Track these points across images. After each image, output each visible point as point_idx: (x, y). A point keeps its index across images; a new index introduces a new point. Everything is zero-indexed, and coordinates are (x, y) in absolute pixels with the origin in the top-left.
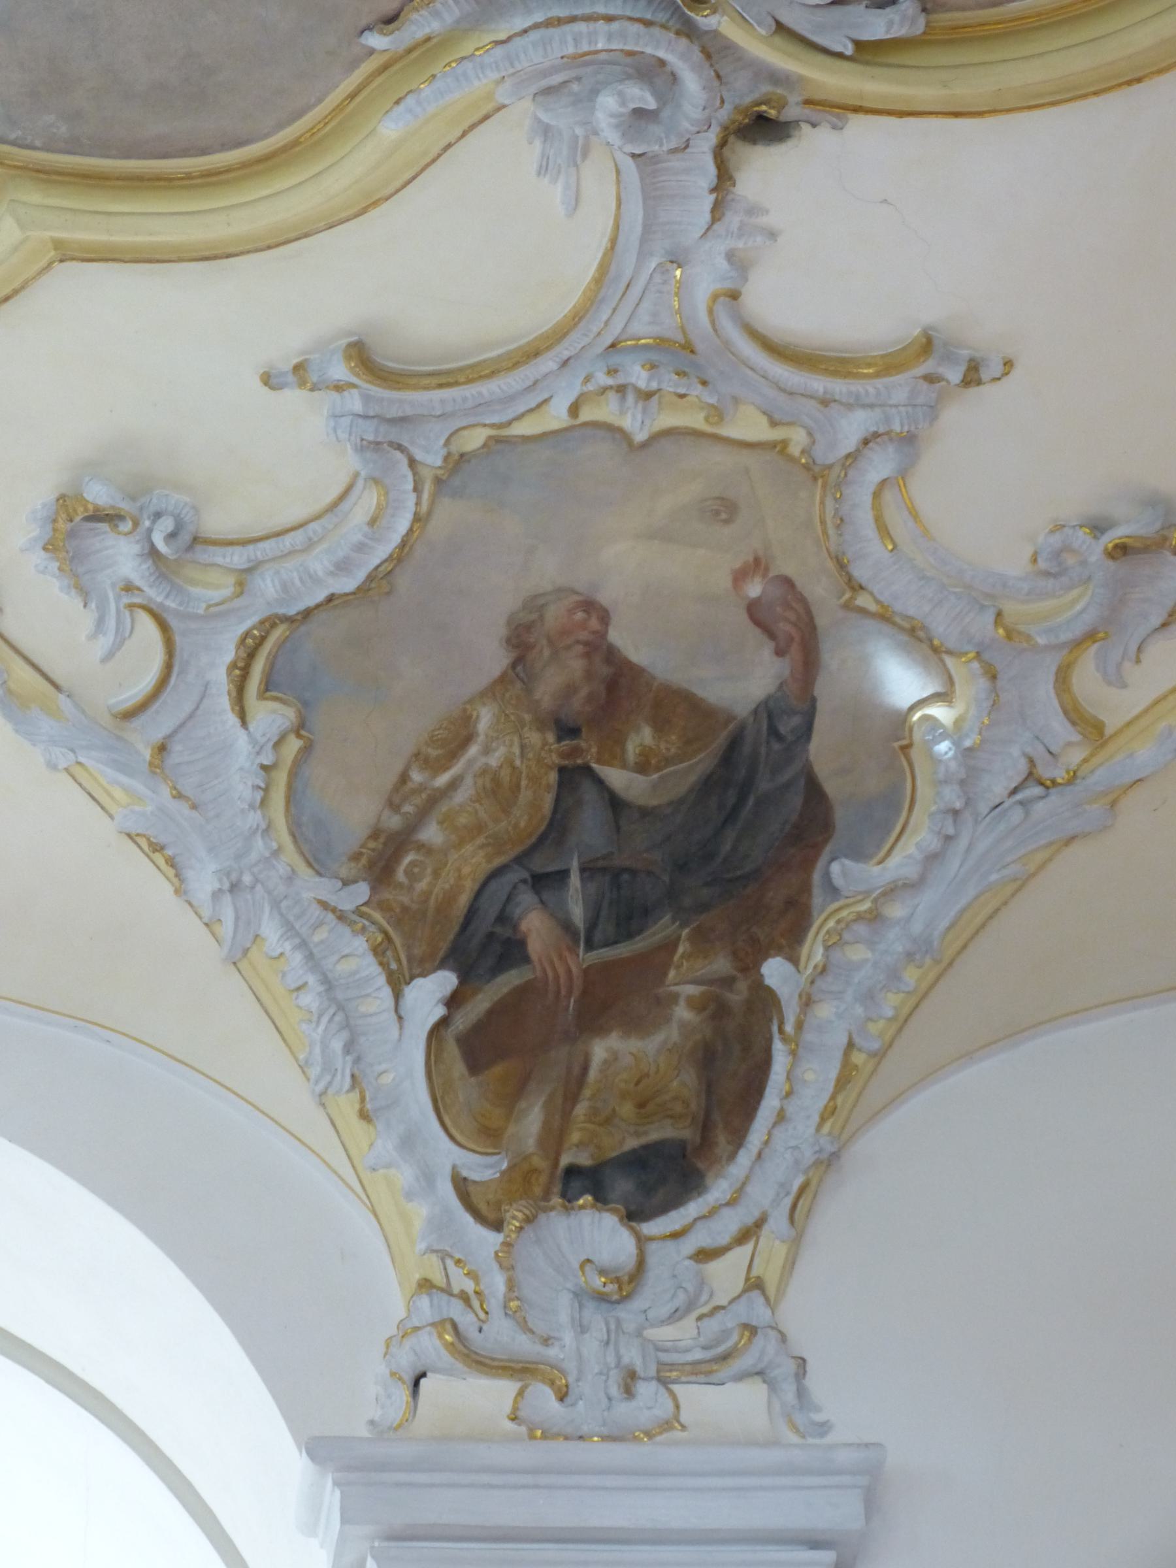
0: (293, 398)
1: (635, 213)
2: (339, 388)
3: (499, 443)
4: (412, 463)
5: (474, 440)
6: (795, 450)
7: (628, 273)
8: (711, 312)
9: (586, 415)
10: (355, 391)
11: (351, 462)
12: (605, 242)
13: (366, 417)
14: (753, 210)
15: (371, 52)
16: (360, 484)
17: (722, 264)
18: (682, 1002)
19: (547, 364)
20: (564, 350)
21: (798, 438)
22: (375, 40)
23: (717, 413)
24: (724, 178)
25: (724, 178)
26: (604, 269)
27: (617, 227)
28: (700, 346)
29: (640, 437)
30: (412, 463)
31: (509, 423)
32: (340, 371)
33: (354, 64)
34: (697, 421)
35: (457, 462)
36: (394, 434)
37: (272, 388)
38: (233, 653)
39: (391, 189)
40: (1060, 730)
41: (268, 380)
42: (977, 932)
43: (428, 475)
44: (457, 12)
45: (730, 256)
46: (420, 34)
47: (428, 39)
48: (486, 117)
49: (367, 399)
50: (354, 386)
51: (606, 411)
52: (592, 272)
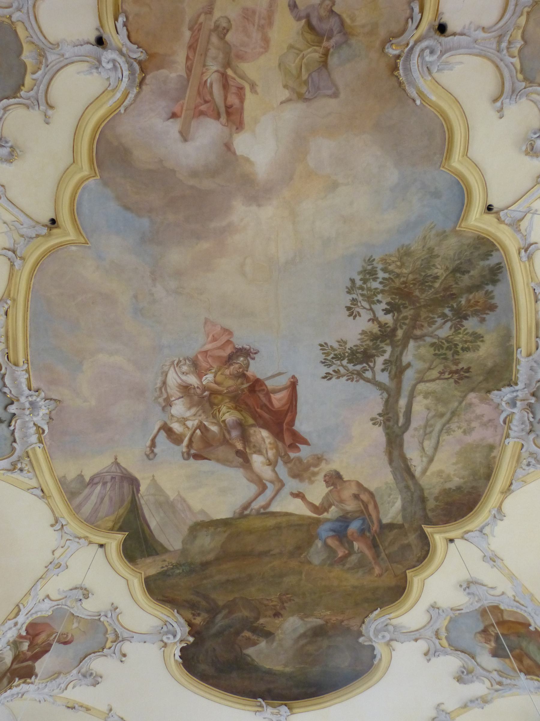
0: (506, 112)
1: (462, 51)
2: (502, 104)
3: (522, 71)
4: (525, 88)
5: (520, 77)
6: (529, 9)
7: (478, 50)
8: (490, 33)
9: (516, 53)
10: (504, 101)
11: (524, 99)
12: (471, 56)
13: (510, 99)
14: (464, 28)
15: (421, 103)
16: (529, 98)
17: (477, 32)
18: (380, 280)
19: (502, 64)
20: (498, 61)
21: (526, 9)
22: (418, 102)
23: (519, 27)
24: (454, 34)
25: (454, 34)
26: (477, 55)
27: (466, 54)
28: (500, 33)
29: (522, 43)
30: (525, 88)
31: (516, 68)
32: (498, 104)
33: (424, 105)
34: (520, 32)
35: (525, 79)
36: (516, 93)
37: (503, 117)
38: (501, 216)
39: (453, 98)
40: (431, 612)
41: (501, 118)
42: (527, 192)
43: (528, 85)
44: (412, 89)
45: (475, 30)
46: (417, 95)
47: (417, 93)
48: (436, 81)
49: (506, 98)
50: (503, 101)
51: (515, 50)
52: (479, 58)
